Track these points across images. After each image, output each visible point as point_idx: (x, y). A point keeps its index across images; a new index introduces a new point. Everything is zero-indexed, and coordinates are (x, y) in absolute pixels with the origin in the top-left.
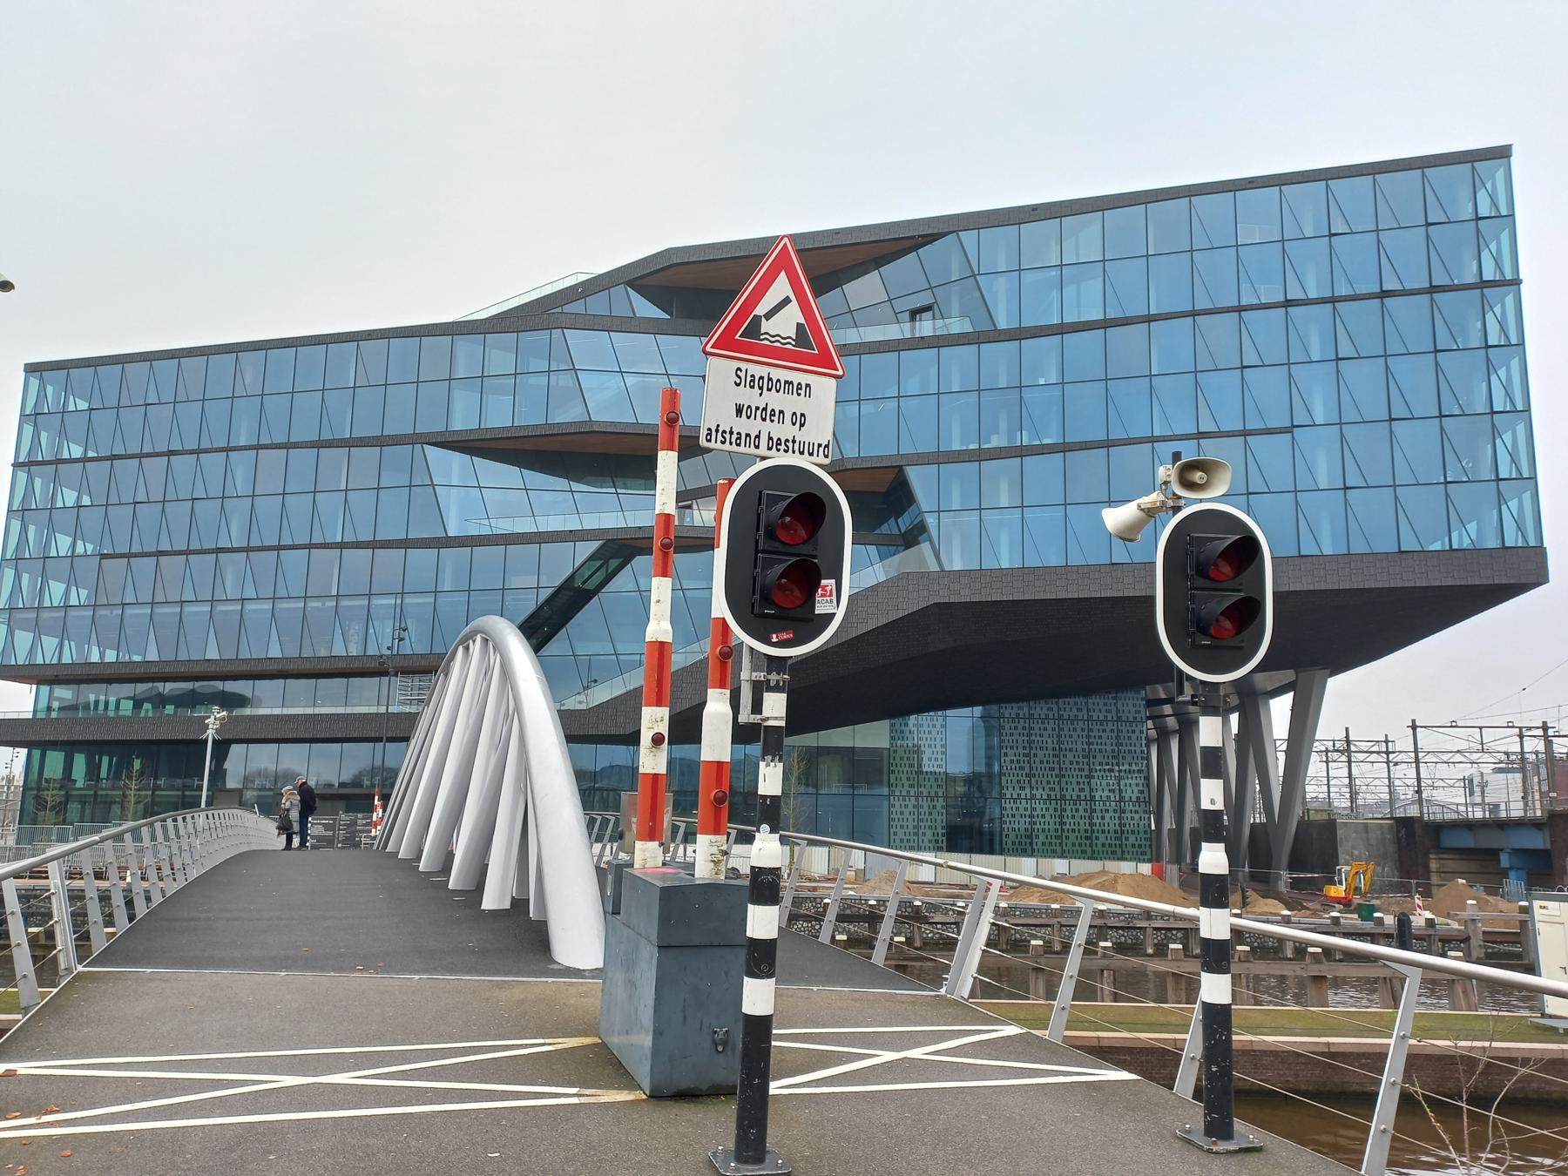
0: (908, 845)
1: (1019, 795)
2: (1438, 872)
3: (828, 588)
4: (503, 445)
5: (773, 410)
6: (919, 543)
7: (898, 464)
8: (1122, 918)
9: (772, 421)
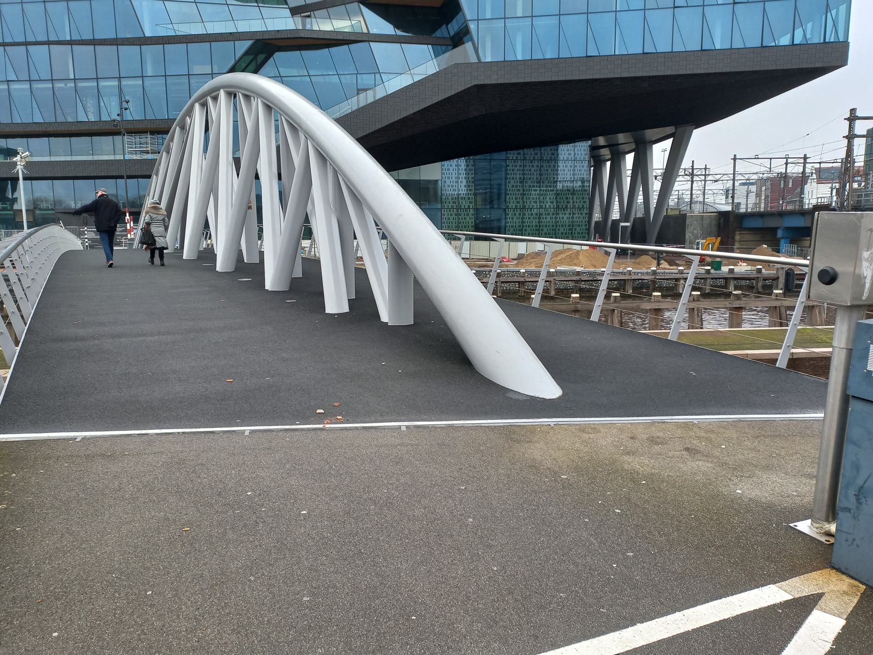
1: (583, 206)
2: (740, 241)
6: (463, 43)
8: (584, 275)
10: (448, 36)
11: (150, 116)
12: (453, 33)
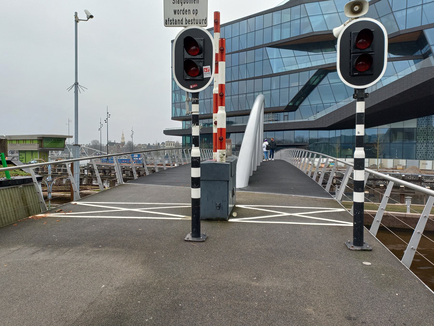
0: (423, 158)
3: (208, 69)
4: (290, 43)
5: (186, 10)
6: (429, 57)
7: (421, 29)
9: (186, 14)
10: (421, 54)
11: (272, 106)
12: (423, 53)
